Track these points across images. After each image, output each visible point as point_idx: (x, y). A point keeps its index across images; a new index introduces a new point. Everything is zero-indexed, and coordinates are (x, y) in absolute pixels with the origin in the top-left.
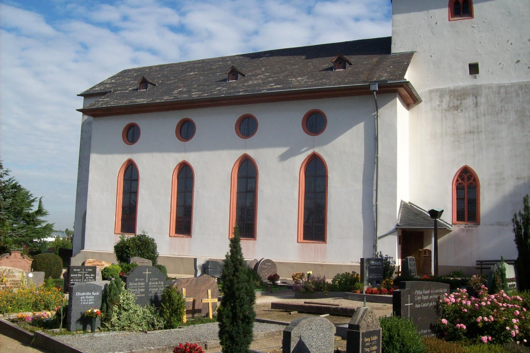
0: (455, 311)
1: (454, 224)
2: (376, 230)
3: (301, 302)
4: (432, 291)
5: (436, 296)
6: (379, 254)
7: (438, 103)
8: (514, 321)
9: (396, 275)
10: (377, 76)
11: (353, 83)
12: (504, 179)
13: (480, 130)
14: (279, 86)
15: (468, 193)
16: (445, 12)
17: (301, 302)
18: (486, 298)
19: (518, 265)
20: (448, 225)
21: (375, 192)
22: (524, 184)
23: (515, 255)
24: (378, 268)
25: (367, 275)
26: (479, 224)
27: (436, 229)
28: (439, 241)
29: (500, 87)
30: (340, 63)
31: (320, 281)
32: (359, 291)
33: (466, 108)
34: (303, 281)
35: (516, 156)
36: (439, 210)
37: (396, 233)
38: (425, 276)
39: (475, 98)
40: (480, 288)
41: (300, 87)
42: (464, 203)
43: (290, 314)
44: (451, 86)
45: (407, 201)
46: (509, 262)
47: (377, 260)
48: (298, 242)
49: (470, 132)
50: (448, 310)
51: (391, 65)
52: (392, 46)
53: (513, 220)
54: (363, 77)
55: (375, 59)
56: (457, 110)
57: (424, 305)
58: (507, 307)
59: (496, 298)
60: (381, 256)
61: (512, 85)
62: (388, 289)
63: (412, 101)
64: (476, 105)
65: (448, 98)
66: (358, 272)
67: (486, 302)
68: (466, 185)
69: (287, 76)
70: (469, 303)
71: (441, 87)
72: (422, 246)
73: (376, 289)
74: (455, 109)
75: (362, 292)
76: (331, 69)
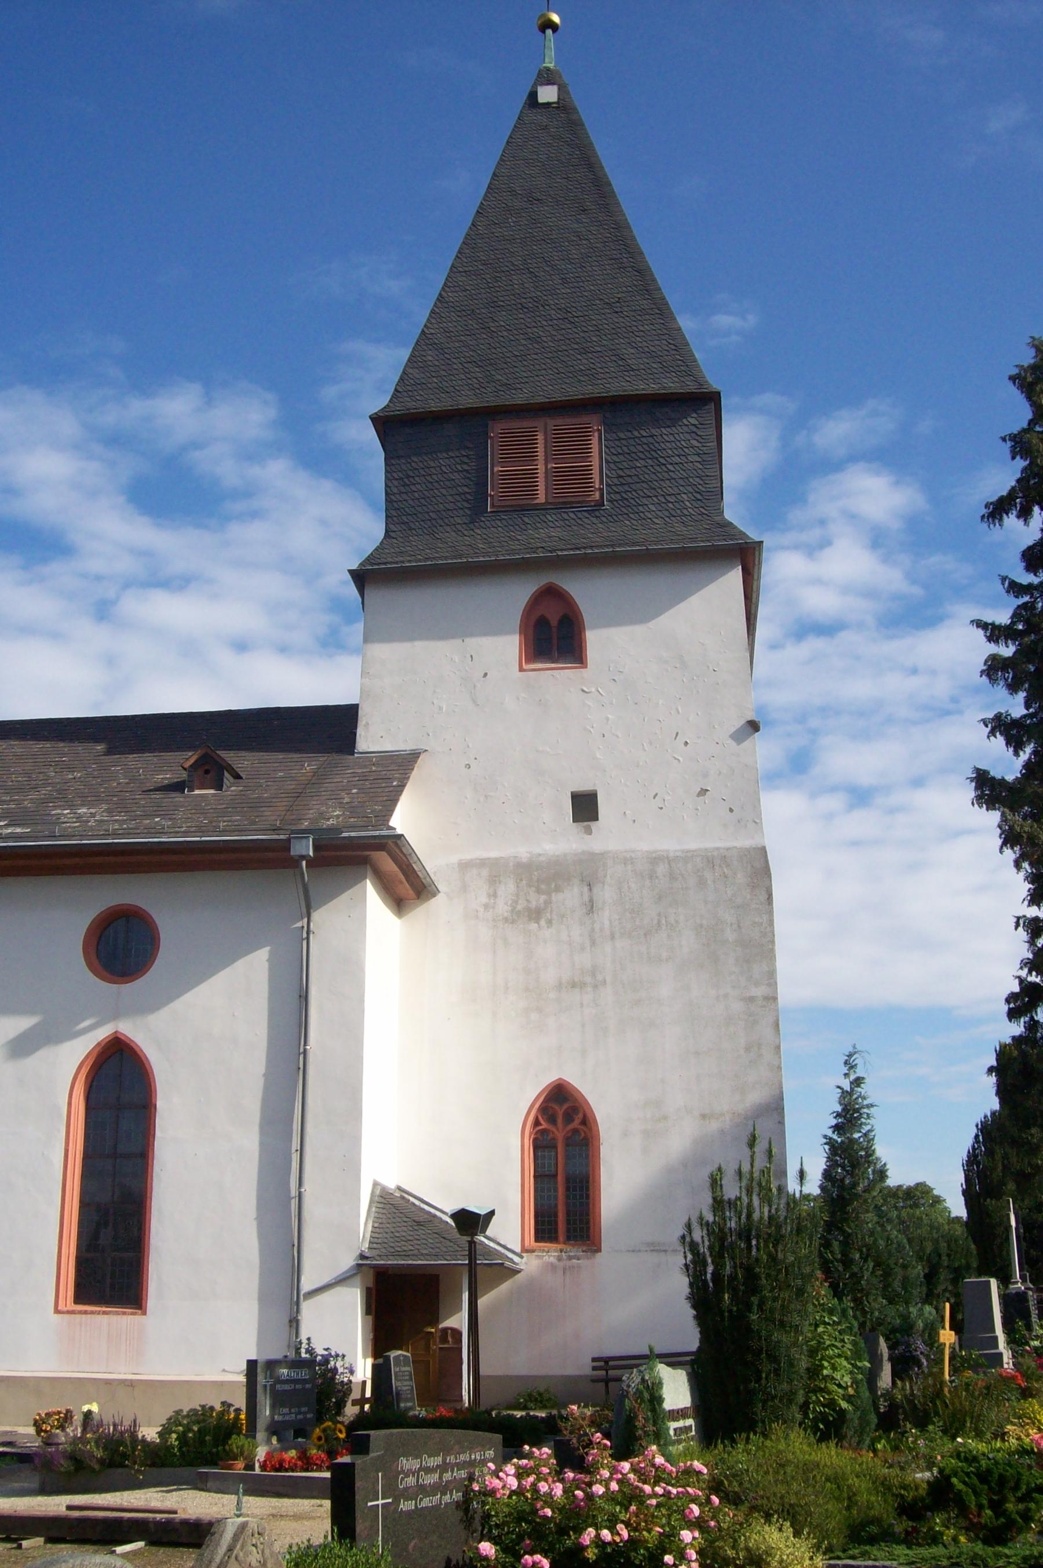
0: (520, 1517)
1: (527, 1251)
2: (297, 1271)
3: (56, 1505)
4: (451, 1459)
5: (463, 1474)
6: (304, 1346)
7: (484, 899)
8: (686, 1535)
9: (356, 1409)
10: (312, 814)
11: (241, 832)
12: (665, 1118)
13: (600, 977)
14: (19, 830)
15: (567, 1157)
16: (509, 646)
17: (56, 1505)
18: (606, 1473)
19: (703, 1371)
20: (510, 1255)
21: (295, 1158)
22: (722, 1132)
23: (690, 1339)
24: (299, 1389)
25: (265, 1411)
26: (599, 1250)
27: (472, 1267)
28: (482, 1302)
29: (655, 859)
30: (207, 772)
31: (122, 1433)
32: (240, 1464)
33: (563, 916)
34: (67, 1435)
35: (697, 1053)
36: (483, 1212)
37: (358, 1280)
38: (443, 1411)
39: (586, 889)
40: (590, 1444)
41: (82, 837)
42: (556, 1190)
43: (20, 1547)
44: (522, 851)
45: (391, 1184)
46: (673, 1360)
47: (297, 1364)
48: (57, 1311)
49: (573, 985)
50: (497, 1515)
51: (355, 786)
52: (360, 731)
53: (683, 1237)
54: (271, 816)
55: (309, 765)
56: (537, 920)
57: (426, 1502)
58: (667, 1494)
59: (634, 1469)
60: (310, 1351)
61: (688, 857)
62: (332, 1454)
63: (411, 892)
64: (591, 907)
65: (511, 887)
66: (240, 1401)
67: (606, 1483)
68: (562, 1134)
69: (44, 802)
70: (558, 1490)
71: (494, 854)
72: (435, 1321)
73: (293, 1453)
74: (530, 919)
75: (250, 1467)
76: (178, 787)
